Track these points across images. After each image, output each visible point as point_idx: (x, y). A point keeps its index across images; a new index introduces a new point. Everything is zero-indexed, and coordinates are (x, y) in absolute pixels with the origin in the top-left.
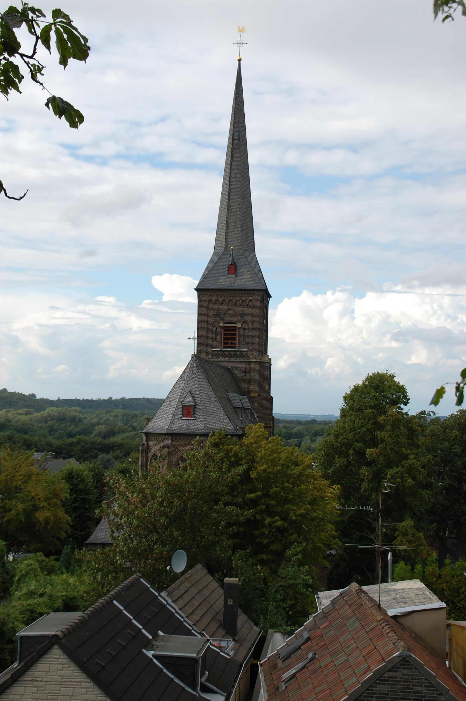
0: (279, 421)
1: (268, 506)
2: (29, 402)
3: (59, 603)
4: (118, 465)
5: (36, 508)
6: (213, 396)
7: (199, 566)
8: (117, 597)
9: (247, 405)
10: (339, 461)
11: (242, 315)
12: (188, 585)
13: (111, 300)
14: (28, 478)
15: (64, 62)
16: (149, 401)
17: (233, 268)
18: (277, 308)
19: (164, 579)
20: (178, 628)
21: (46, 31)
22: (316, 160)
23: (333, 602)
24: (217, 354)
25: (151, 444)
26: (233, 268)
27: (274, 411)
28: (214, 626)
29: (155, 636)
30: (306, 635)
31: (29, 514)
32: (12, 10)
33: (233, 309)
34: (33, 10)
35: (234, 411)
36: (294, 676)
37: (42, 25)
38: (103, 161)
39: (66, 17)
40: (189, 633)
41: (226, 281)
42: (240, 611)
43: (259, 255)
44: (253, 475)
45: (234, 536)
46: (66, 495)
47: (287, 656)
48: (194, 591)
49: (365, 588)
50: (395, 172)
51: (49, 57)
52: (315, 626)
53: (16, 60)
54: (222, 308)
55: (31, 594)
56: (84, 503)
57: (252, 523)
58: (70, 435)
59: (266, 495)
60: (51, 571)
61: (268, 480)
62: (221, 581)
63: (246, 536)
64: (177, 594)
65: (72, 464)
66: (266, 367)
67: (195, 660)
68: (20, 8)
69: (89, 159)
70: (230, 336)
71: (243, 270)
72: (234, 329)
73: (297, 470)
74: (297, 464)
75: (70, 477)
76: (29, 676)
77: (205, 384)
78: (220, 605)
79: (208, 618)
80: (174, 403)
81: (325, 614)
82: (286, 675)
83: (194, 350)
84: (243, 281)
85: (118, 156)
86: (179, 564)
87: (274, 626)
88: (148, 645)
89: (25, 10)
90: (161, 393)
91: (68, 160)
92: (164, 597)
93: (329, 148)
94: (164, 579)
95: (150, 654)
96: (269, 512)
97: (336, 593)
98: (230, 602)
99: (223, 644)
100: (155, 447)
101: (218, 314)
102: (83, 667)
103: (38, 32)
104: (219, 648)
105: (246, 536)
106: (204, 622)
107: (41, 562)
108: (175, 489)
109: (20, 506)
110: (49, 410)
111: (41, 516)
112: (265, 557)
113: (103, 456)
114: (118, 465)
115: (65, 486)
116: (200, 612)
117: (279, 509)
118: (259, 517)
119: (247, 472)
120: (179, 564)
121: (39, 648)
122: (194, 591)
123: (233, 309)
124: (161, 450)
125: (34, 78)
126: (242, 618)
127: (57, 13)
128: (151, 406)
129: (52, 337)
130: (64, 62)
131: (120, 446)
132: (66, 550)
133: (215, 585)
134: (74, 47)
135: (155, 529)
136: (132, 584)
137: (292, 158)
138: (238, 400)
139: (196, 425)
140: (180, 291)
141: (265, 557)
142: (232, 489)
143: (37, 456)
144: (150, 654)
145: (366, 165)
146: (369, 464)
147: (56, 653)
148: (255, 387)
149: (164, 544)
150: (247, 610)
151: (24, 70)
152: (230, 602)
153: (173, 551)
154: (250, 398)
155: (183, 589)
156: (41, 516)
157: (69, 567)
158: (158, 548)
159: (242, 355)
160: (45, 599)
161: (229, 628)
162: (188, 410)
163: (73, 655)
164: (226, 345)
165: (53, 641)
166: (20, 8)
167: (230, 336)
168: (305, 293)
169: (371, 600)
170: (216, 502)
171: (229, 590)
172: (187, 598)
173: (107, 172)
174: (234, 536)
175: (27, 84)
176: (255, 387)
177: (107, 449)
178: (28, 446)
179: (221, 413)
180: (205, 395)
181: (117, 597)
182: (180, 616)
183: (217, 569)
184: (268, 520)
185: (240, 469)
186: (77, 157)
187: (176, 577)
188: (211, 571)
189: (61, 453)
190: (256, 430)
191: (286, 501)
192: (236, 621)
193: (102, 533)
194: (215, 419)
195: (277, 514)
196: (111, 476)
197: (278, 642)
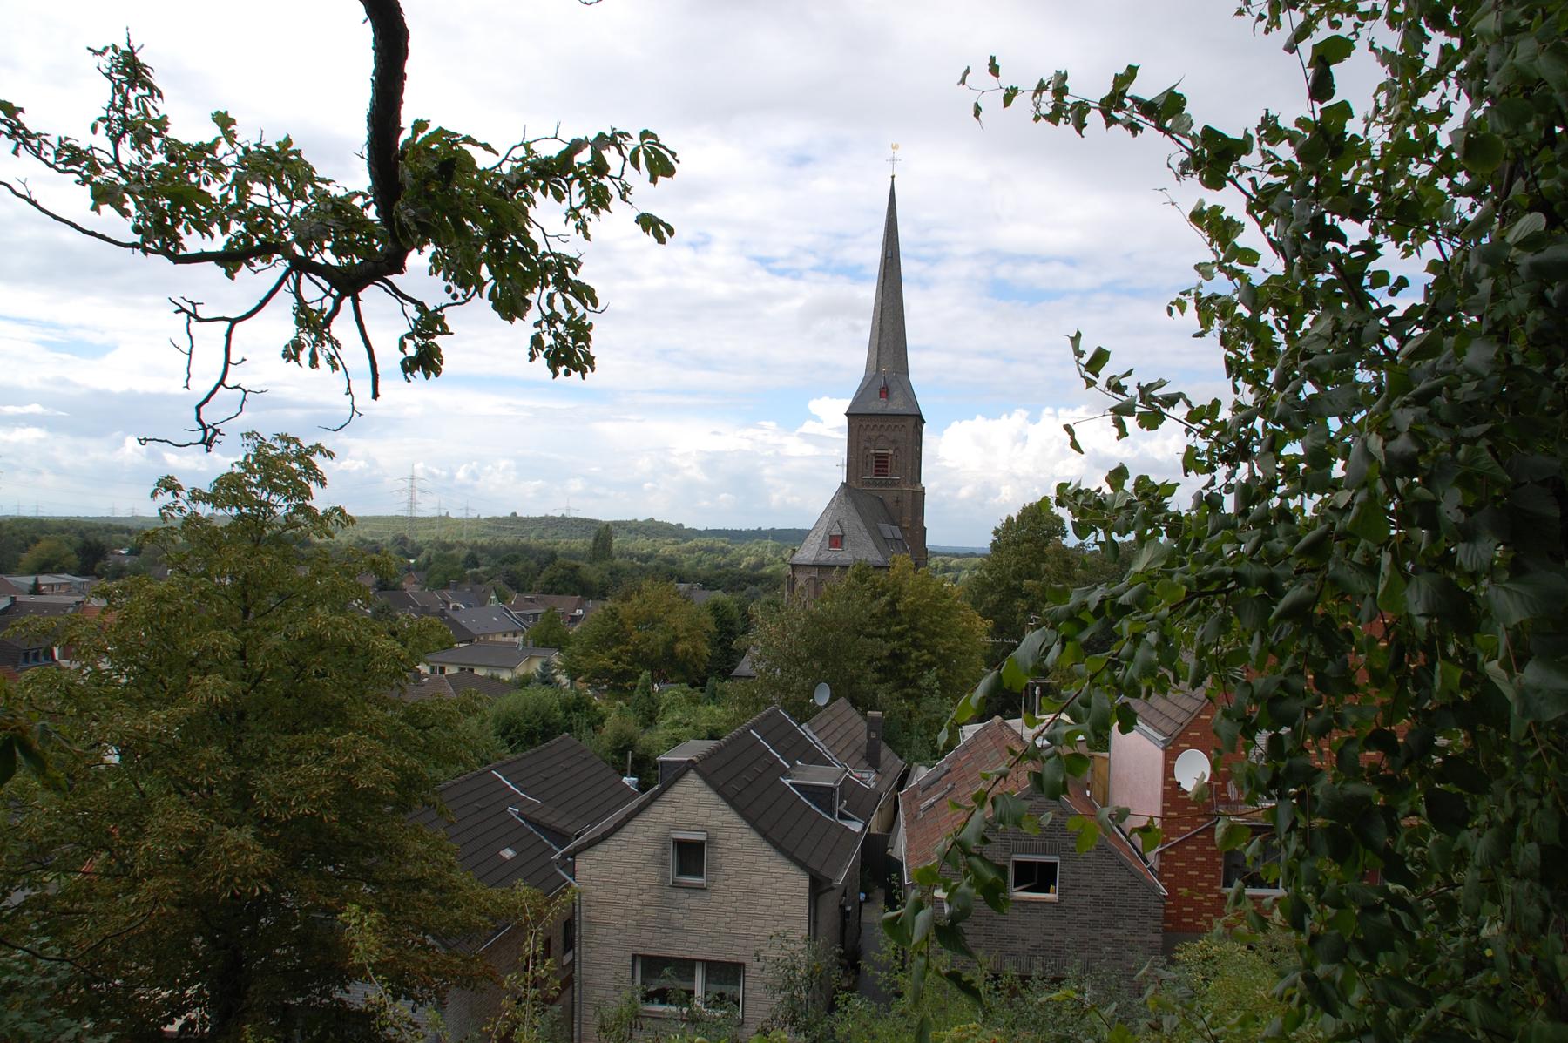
0: (935, 554)
1: (915, 639)
2: (677, 533)
3: (704, 733)
4: (766, 597)
5: (677, 639)
6: (861, 525)
7: (842, 700)
8: (753, 726)
9: (899, 536)
10: (992, 598)
11: (894, 442)
12: (830, 717)
13: (772, 424)
14: (670, 609)
15: (653, 180)
16: (800, 531)
17: (885, 392)
18: (941, 435)
19: (804, 712)
20: (817, 758)
21: (635, 154)
22: (1032, 272)
23: (975, 735)
24: (868, 483)
25: (798, 576)
26: (885, 392)
27: (928, 543)
28: (857, 758)
29: (793, 765)
30: (946, 767)
31: (669, 646)
32: (601, 136)
33: (885, 436)
34: (621, 134)
35: (884, 542)
36: (932, 805)
37: (631, 148)
38: (797, 275)
39: (654, 136)
40: (828, 763)
41: (877, 406)
42: (883, 744)
43: (913, 377)
44: (900, 607)
45: (879, 670)
46: (712, 628)
47: (926, 788)
48: (836, 723)
49: (1009, 722)
50: (1113, 288)
51: (638, 179)
52: (957, 758)
53: (605, 181)
54: (875, 434)
55: (676, 724)
56: (728, 634)
57: (896, 656)
58: (718, 566)
59: (914, 629)
60: (697, 702)
61: (915, 613)
62: (864, 714)
63: (894, 670)
64: (818, 727)
65: (719, 595)
66: (918, 497)
67: (832, 789)
68: (609, 134)
69: (782, 273)
70: (881, 463)
71: (895, 393)
72: (886, 456)
73: (946, 603)
74: (945, 596)
75: (715, 608)
76: (666, 797)
77: (854, 514)
78: (863, 738)
79: (851, 750)
80: (822, 534)
81: (967, 747)
82: (923, 806)
83: (841, 476)
84: (896, 405)
85: (815, 269)
86: (822, 697)
87: (918, 759)
88: (785, 773)
89: (614, 136)
90: (808, 525)
91: (760, 274)
92: (805, 729)
93: (1044, 260)
94: (804, 712)
95: (787, 782)
96: (916, 644)
97: (980, 726)
98: (873, 736)
99: (865, 775)
100: (801, 579)
101: (869, 440)
102: (719, 791)
103: (627, 154)
104: (861, 779)
105: (894, 670)
106: (846, 755)
107: (685, 693)
108: (815, 620)
109: (660, 637)
110: (703, 542)
111: (680, 647)
112: (910, 691)
113: (751, 588)
114: (766, 597)
115: (711, 619)
116: (843, 744)
117: (927, 643)
118: (905, 650)
119: (892, 603)
120: (822, 697)
121: (678, 771)
122: (836, 723)
123: (885, 436)
124: (807, 582)
125: (623, 198)
126: (885, 752)
127: (645, 134)
128: (796, 537)
129: (710, 462)
130: (653, 180)
131: (768, 578)
132: (711, 681)
133: (859, 718)
134: (661, 166)
135: (798, 662)
136: (769, 715)
137: (1003, 271)
138: (888, 530)
139: (843, 556)
140: (830, 420)
141: (910, 691)
142: (879, 620)
143: (683, 586)
144: (787, 782)
145: (1082, 279)
146: (1025, 596)
147: (692, 776)
148: (907, 517)
149: (806, 676)
150: (891, 743)
151: (613, 190)
152: (873, 736)
153: (816, 683)
154: (902, 529)
155: (825, 721)
156: (680, 647)
157: (714, 697)
158: (800, 681)
159: (893, 483)
160: (690, 728)
161: (872, 760)
162: (836, 541)
163: (708, 779)
164: (877, 472)
165: (690, 765)
166: (609, 134)
167: (881, 463)
168: (979, 417)
169: (1014, 732)
170: (859, 633)
171: (872, 723)
172: (829, 730)
173: (801, 286)
174: (879, 670)
175: (615, 203)
176: (907, 517)
177: (755, 581)
178: (671, 576)
179: (871, 544)
180: (854, 525)
181: (753, 726)
182: (822, 747)
183: (861, 703)
184: (915, 654)
185: (885, 599)
186: (771, 271)
187: (819, 709)
188: (854, 703)
189: (708, 584)
190: (903, 560)
191: (935, 634)
192: (878, 753)
193: (744, 667)
194: (862, 550)
195: (925, 647)
196: (755, 609)
197: (921, 773)
